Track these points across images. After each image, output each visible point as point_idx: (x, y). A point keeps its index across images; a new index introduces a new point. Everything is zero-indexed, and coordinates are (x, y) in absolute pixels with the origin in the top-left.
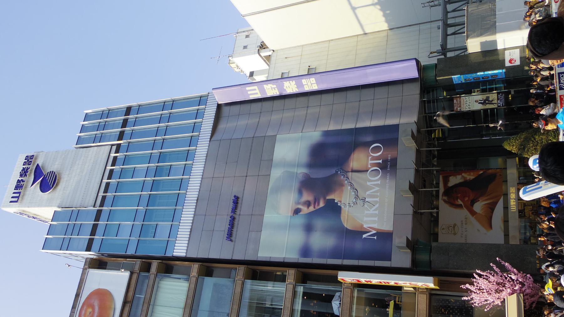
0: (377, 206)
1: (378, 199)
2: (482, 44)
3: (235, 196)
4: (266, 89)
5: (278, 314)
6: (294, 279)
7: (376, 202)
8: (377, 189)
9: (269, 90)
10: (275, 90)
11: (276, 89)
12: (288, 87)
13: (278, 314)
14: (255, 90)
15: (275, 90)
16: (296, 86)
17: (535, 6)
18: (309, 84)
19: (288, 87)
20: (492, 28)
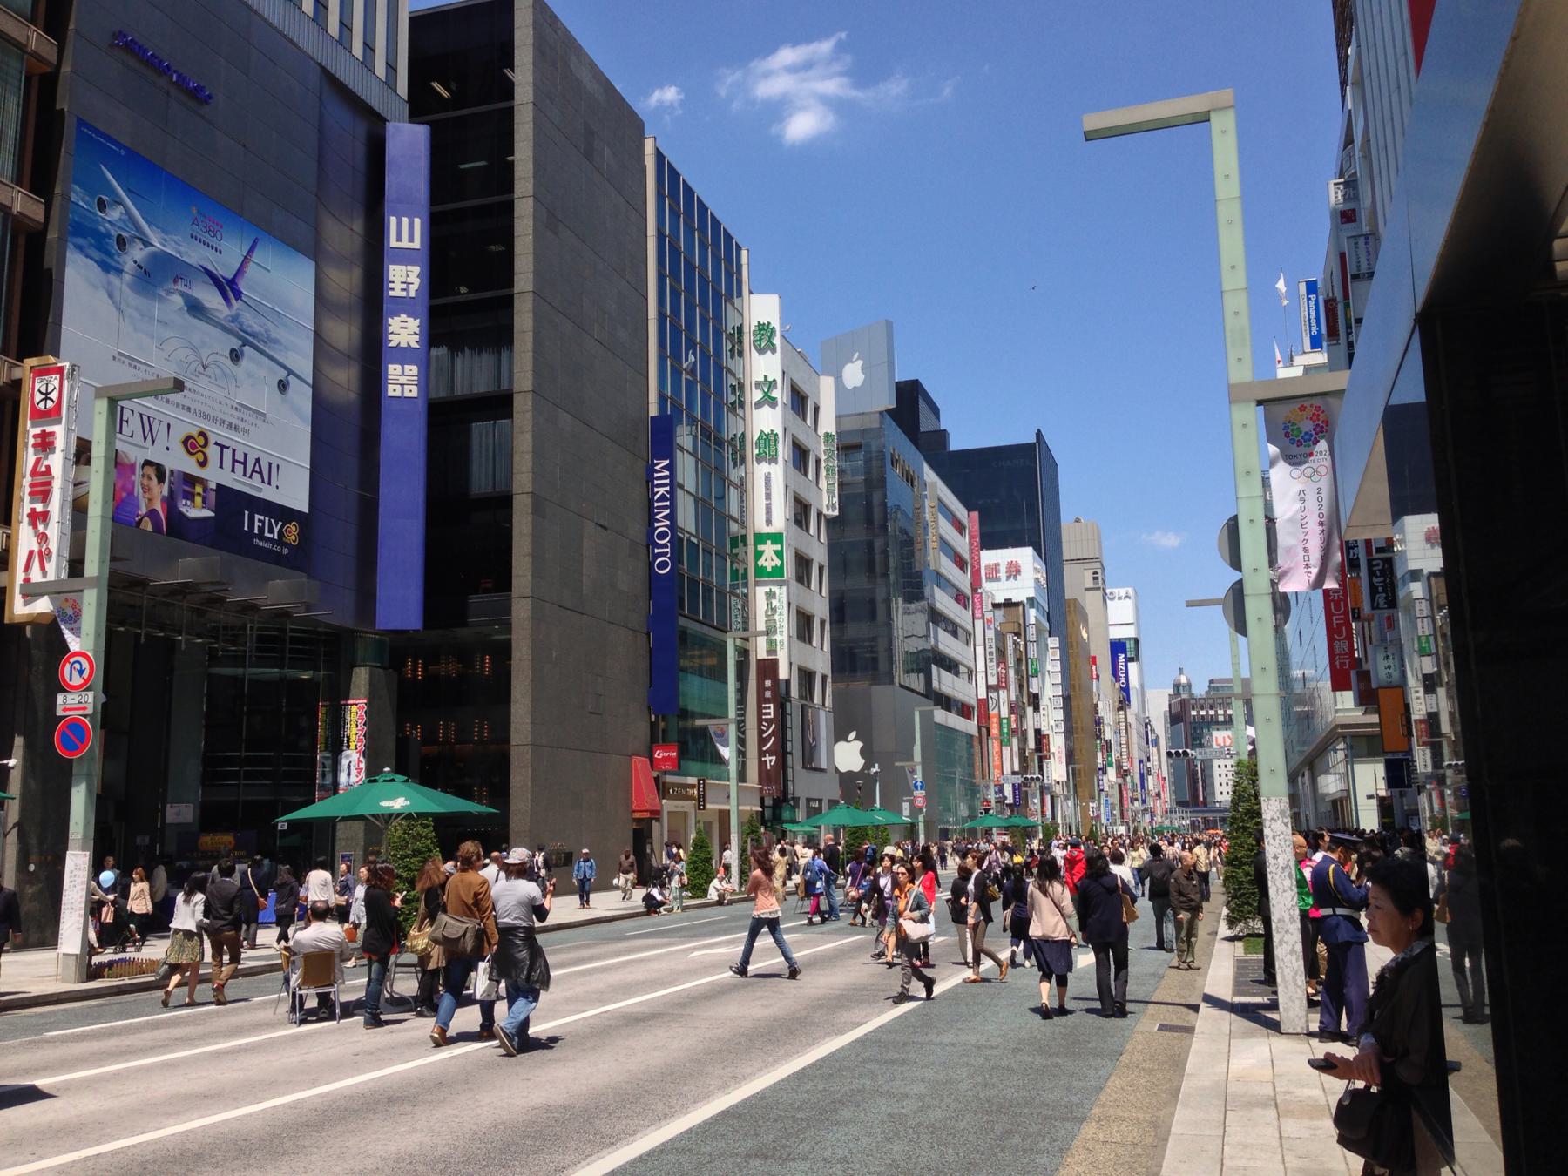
0: (656, 497)
1: (656, 504)
2: (1470, 1017)
3: (210, 97)
4: (410, 268)
5: (487, 450)
6: (1357, 813)
7: (658, 501)
8: (658, 517)
9: (405, 275)
10: (402, 290)
11: (404, 294)
12: (404, 325)
13: (487, 450)
14: (411, 239)
15: (402, 290)
16: (404, 345)
17: (1054, 642)
18: (403, 380)
19: (404, 325)
20: (1104, 857)
